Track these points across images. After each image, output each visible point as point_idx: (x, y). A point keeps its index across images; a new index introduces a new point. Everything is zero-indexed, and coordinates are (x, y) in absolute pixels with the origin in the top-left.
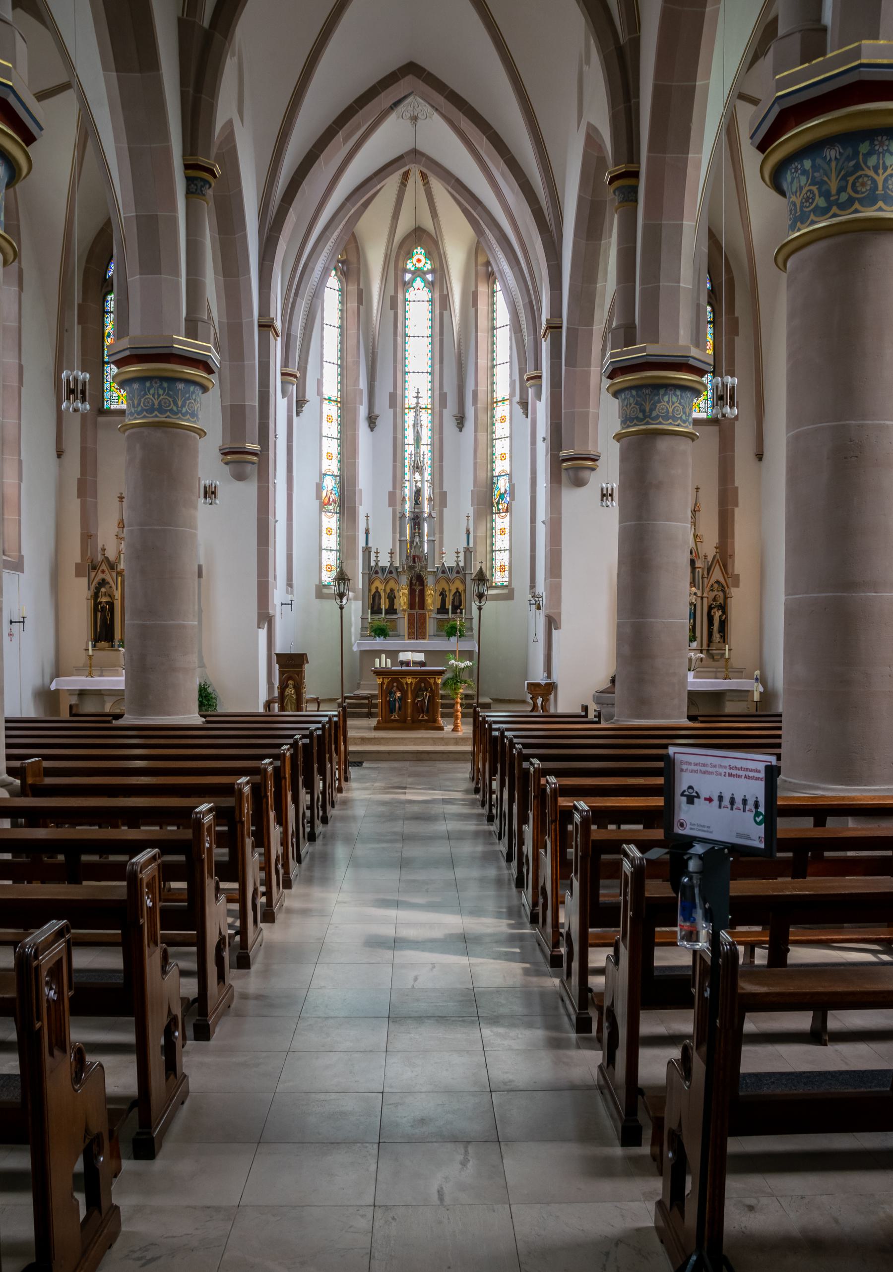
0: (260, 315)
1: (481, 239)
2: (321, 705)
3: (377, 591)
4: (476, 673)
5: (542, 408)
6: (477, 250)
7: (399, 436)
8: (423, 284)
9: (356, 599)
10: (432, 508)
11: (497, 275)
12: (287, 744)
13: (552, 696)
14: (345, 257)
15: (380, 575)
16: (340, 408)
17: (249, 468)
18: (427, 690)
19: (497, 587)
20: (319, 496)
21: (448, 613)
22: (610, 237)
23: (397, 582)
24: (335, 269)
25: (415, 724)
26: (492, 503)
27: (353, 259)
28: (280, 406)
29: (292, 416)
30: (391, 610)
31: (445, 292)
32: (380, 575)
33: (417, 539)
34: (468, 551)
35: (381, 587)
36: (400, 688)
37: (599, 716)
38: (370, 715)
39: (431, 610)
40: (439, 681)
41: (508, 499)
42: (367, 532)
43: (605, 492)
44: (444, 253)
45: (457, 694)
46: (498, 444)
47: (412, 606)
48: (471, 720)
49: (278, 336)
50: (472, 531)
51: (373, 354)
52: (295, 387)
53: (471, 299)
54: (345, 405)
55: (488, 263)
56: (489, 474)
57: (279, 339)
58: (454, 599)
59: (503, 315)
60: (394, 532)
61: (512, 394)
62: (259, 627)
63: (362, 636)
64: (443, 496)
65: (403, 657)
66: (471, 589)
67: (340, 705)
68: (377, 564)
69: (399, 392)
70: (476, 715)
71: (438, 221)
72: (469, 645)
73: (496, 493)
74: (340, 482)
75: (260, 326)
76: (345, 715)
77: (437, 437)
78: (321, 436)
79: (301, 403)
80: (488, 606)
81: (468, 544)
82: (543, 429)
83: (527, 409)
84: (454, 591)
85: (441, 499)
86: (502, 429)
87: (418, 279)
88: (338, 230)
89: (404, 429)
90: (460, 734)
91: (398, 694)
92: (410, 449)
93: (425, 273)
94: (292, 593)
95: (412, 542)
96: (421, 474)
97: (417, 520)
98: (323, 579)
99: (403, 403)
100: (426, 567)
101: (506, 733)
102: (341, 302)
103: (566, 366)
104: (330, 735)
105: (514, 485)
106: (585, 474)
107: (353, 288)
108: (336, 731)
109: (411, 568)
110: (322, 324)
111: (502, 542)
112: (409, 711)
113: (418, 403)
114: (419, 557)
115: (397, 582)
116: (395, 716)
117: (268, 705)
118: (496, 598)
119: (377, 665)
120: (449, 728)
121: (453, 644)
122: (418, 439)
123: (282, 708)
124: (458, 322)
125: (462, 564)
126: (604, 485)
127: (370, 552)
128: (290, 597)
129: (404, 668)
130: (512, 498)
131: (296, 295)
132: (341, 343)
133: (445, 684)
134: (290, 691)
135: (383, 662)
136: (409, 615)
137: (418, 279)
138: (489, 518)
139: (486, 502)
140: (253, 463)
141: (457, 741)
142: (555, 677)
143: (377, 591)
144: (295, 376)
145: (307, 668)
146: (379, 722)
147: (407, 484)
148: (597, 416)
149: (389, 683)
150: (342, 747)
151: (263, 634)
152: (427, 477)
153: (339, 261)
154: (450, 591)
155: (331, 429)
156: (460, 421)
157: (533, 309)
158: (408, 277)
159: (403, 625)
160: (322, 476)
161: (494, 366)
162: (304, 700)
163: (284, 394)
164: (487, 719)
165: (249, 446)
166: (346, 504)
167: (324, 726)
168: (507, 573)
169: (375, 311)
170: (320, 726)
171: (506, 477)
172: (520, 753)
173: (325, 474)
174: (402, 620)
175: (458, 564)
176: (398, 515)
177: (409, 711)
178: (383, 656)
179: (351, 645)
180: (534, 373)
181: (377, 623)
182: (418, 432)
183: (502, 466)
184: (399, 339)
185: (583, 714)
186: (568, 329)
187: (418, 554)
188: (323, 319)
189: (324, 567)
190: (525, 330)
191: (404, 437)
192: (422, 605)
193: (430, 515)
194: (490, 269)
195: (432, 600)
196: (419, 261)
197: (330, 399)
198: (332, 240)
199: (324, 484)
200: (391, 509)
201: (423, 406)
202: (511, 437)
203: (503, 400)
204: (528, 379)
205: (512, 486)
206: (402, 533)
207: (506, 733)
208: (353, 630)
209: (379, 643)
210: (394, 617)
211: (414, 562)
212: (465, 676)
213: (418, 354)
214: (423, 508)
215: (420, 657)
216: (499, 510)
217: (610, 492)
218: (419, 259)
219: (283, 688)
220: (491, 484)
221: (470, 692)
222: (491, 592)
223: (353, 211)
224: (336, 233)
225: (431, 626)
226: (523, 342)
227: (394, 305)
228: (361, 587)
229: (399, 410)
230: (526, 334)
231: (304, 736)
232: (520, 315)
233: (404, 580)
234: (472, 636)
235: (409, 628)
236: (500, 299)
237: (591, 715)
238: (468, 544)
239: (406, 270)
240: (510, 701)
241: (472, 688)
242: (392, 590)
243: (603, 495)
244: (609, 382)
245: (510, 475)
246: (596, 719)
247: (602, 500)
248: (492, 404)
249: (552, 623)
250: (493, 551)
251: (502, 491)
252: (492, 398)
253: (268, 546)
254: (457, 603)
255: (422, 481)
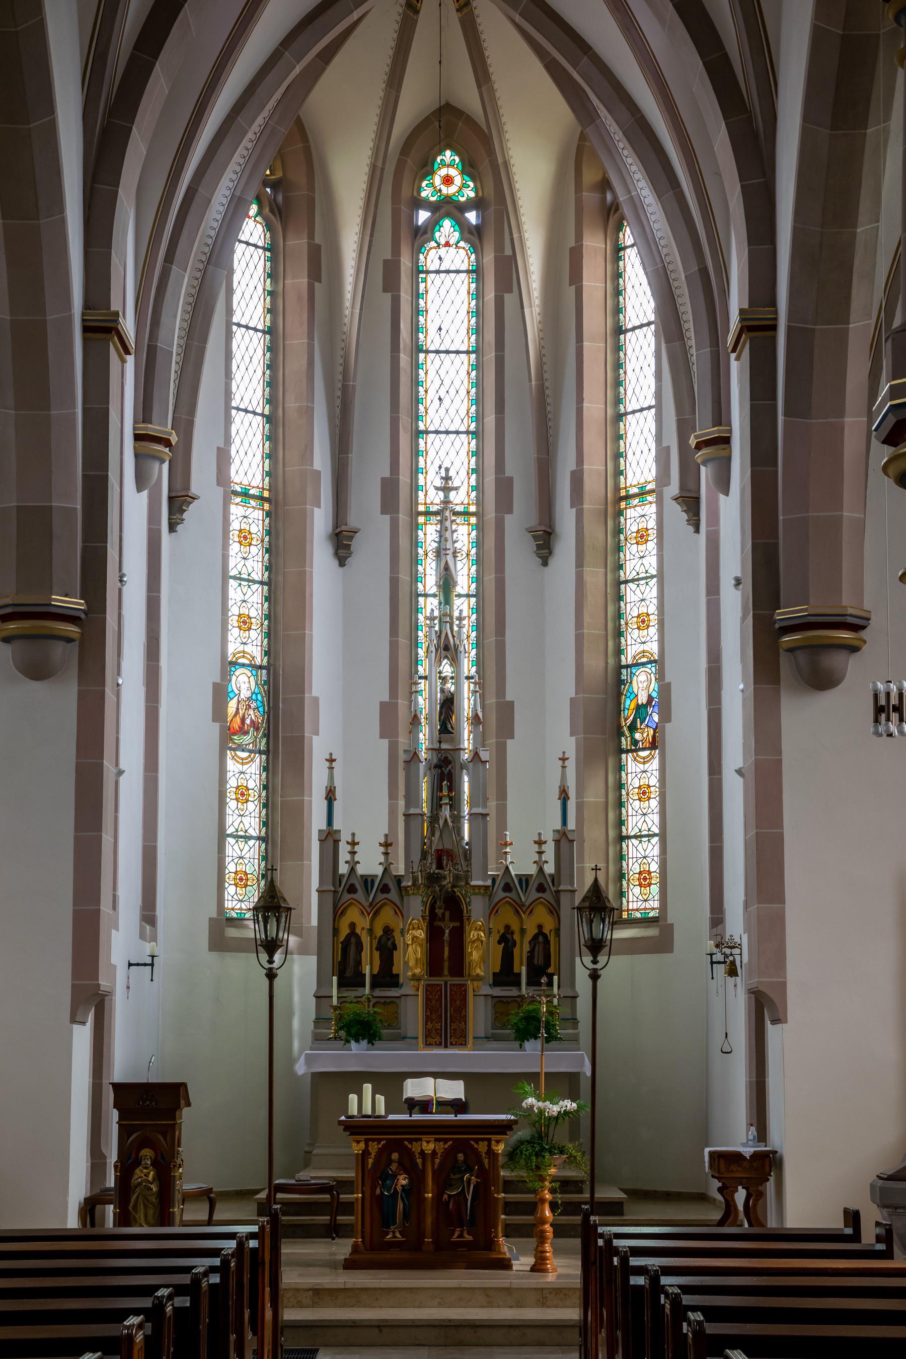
0: (87, 306)
1: (589, 131)
2: (218, 1206)
3: (353, 933)
4: (587, 1129)
5: (731, 511)
6: (580, 159)
7: (404, 577)
8: (457, 235)
9: (303, 950)
10: (481, 740)
11: (626, 210)
12: (136, 1312)
13: (770, 1186)
14: (279, 174)
15: (360, 895)
16: (268, 514)
17: (58, 650)
18: (470, 1170)
19: (632, 922)
20: (219, 712)
21: (518, 984)
22: (887, 117)
23: (399, 911)
24: (259, 200)
25: (443, 1256)
26: (620, 727)
27: (298, 176)
28: (133, 510)
29: (159, 531)
30: (387, 977)
31: (508, 252)
32: (360, 895)
33: (446, 812)
34: (563, 839)
35: (362, 923)
36: (408, 1165)
37: (887, 1236)
38: (333, 1231)
39: (478, 978)
40: (500, 1148)
41: (656, 718)
42: (330, 796)
43: (883, 702)
44: (506, 164)
45: (542, 1179)
46: (631, 593)
47: (434, 965)
48: (577, 1242)
49: (128, 352)
50: (572, 793)
51: (347, 389)
52: (166, 466)
53: (566, 267)
54: (280, 504)
55: (605, 185)
56: (611, 661)
57: (130, 359)
58: (531, 952)
59: (640, 302)
60: (393, 796)
61: (663, 477)
62: (73, 1021)
63: (318, 1039)
64: (506, 711)
65: (414, 1089)
66: (573, 929)
67: (263, 1208)
68: (352, 870)
69: (404, 478)
70: (588, 1233)
71: (492, 91)
72: (572, 1060)
73: (629, 704)
74: (267, 682)
75: (86, 329)
76: (276, 1232)
77: (490, 578)
78: (225, 577)
79: (179, 502)
80: (615, 968)
81: (564, 822)
82: (734, 559)
83: (697, 514)
84: (531, 931)
85: (500, 719)
86: (640, 559)
87: (447, 223)
88: (265, 113)
89: (414, 561)
90: (551, 1278)
91: (403, 1181)
92: (430, 605)
93: (461, 208)
94: (154, 938)
95: (434, 819)
96: (455, 661)
97: (445, 769)
98: (228, 904)
99: (414, 501)
100: (467, 877)
101: (665, 1280)
102: (272, 275)
103: (786, 414)
104: (240, 1284)
105: (669, 685)
106: (835, 660)
107: (298, 243)
108: (254, 1270)
109: (433, 879)
110: (229, 324)
111: (642, 816)
112: (429, 1220)
113: (446, 502)
114: (450, 854)
115: (399, 911)
116: (394, 1235)
117: (90, 1208)
118: (632, 947)
119: (353, 1110)
120: (523, 1263)
121: (531, 1056)
122: (447, 584)
123: (123, 1219)
124: (537, 318)
125: (549, 869)
126: (880, 686)
127: (336, 842)
128: (148, 948)
129: (416, 1117)
130: (666, 716)
131: (169, 258)
132: (271, 366)
133: (512, 1155)
134: (145, 1174)
135: (367, 1102)
136: (429, 989)
137: (447, 223)
138: (611, 762)
139: (608, 726)
140: (69, 640)
141: (544, 1296)
142: (777, 1139)
143: (353, 933)
144: (167, 443)
145: (187, 1117)
146: (355, 1249)
147: (423, 685)
148: (860, 528)
149: (380, 1152)
150: (269, 1314)
151: (82, 1036)
152: (468, 667)
153: (265, 183)
154: (523, 931)
155: (248, 561)
156: (544, 542)
157: (709, 287)
158: (423, 216)
159: (413, 1013)
160: (228, 666)
161: (619, 417)
162: (178, 1197)
163: (141, 482)
164: (616, 1242)
165: (59, 600)
166: (281, 732)
167: (225, 1262)
168: (655, 889)
169: (348, 296)
170: (217, 1262)
171: (651, 669)
172: (699, 1333)
173: (233, 664)
174: (410, 1001)
175: (541, 870)
176: (402, 757)
177: (429, 1220)
178: (368, 1088)
179: (292, 1061)
180: (713, 432)
181: (352, 1008)
182: (447, 568)
183: (640, 643)
184: (404, 358)
185: (849, 1231)
186: (790, 330)
187: (448, 846)
188: (230, 311)
189: (229, 878)
190: (692, 334)
191: (415, 578)
192: (458, 965)
193: (476, 755)
194: (609, 197)
195: (480, 951)
196: (448, 180)
197: (245, 495)
198: (250, 135)
199: (233, 685)
200: (386, 742)
201: (459, 509)
202: (660, 576)
203: (642, 494)
204: (699, 447)
205: (665, 689)
206: (412, 797)
207: (665, 1280)
208: (296, 1024)
209: (357, 1056)
210: (393, 992)
211: (440, 866)
212: (560, 1136)
213: (448, 390)
214: (459, 740)
215: (454, 1090)
216: (635, 742)
217: (894, 701)
218: (448, 178)
219: (126, 1167)
220: (616, 682)
221: (571, 1173)
222: (621, 934)
223: (297, 70)
224: (260, 120)
225: (478, 1015)
226: (687, 361)
227: (391, 283)
228: (314, 922)
229: (403, 517)
230: (693, 342)
231: (179, 1290)
232: (679, 301)
233: (416, 906)
234: (575, 1039)
235: (427, 1019)
236: (633, 267)
237: (869, 1235)
238: (564, 822)
239: (418, 203)
240: (668, 1197)
241: (578, 1165)
242: (388, 931)
243: (879, 710)
244: (887, 452)
245: (659, 663)
246: (881, 1247)
247: (877, 721)
248: (618, 500)
249: (765, 1008)
250: (622, 838)
251: (643, 699)
252: (617, 489)
253: (100, 829)
254: (539, 960)
255: (456, 678)
